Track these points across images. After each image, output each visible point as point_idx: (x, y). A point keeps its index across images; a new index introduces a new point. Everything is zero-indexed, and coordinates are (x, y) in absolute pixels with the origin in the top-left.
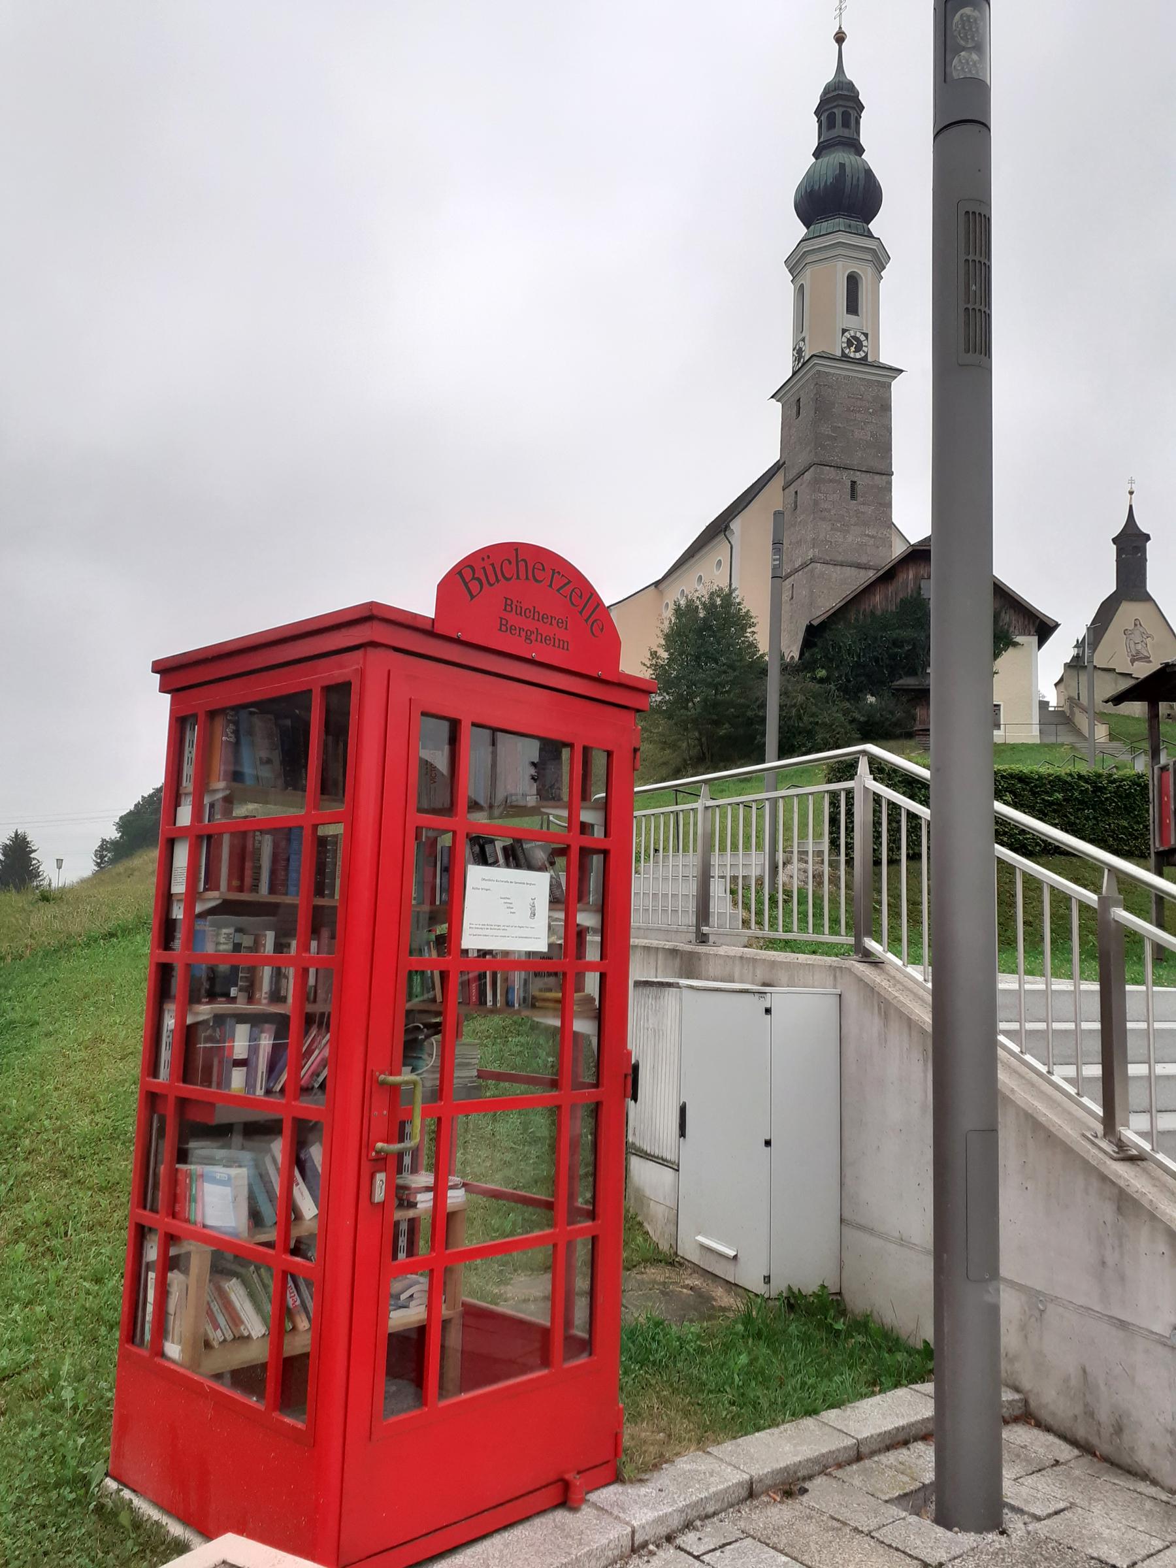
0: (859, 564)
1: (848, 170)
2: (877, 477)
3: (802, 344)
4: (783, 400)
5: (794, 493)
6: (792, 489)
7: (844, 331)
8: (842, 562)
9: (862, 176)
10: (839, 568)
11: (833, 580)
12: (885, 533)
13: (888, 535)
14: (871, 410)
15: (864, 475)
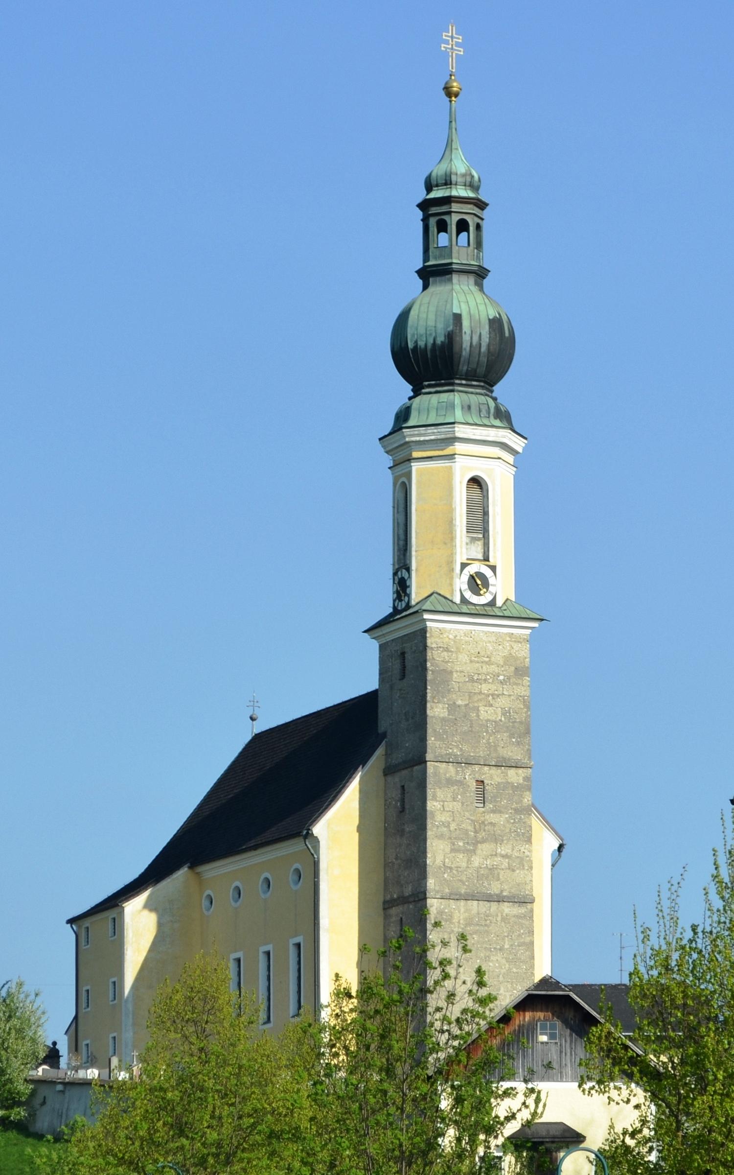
0: (490, 895)
1: (466, 324)
2: (512, 772)
3: (405, 574)
4: (383, 640)
5: (399, 786)
6: (396, 779)
7: (464, 566)
8: (466, 894)
9: (485, 331)
10: (462, 903)
11: (455, 920)
12: (522, 849)
13: (527, 853)
14: (501, 678)
15: (494, 771)
